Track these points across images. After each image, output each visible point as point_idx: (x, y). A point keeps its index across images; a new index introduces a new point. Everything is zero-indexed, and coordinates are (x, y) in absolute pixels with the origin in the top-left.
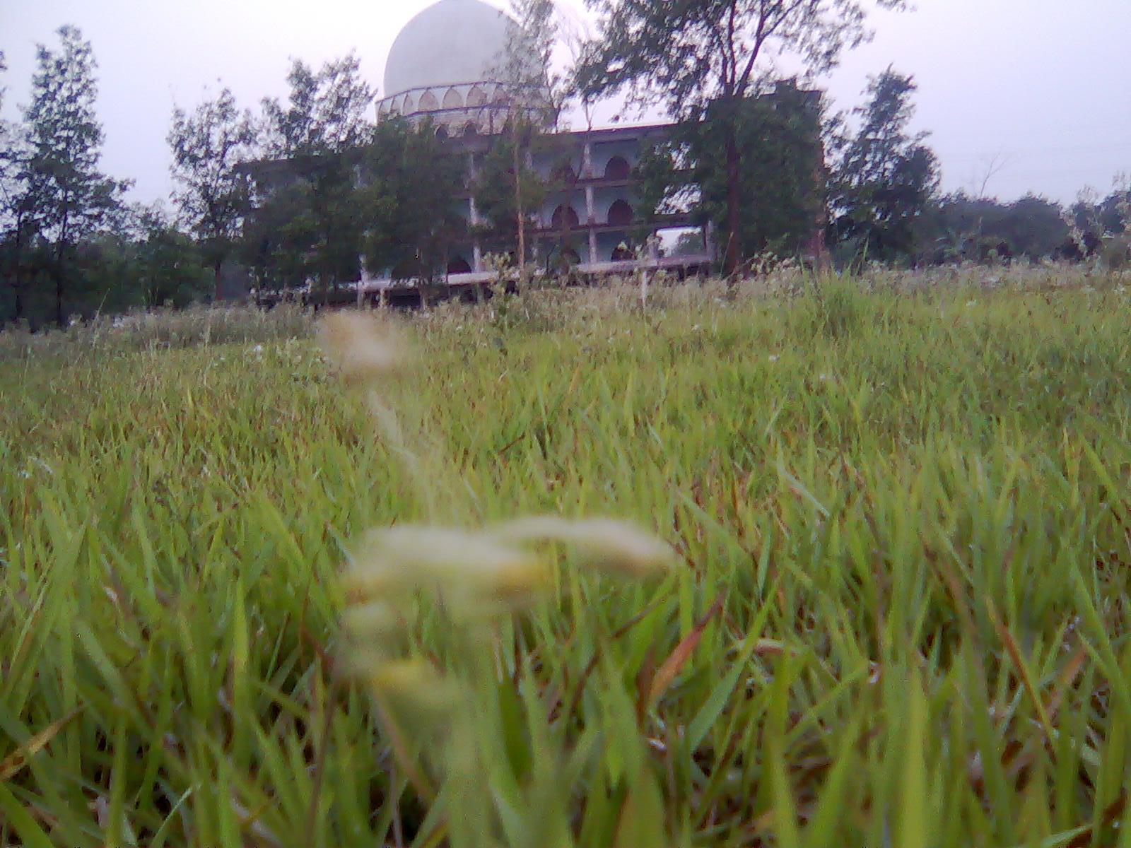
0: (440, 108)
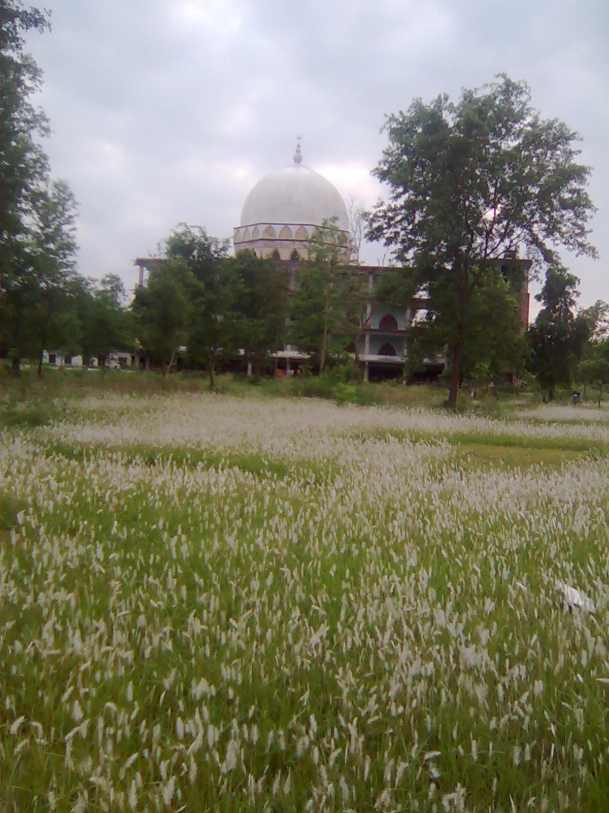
0: (277, 238)
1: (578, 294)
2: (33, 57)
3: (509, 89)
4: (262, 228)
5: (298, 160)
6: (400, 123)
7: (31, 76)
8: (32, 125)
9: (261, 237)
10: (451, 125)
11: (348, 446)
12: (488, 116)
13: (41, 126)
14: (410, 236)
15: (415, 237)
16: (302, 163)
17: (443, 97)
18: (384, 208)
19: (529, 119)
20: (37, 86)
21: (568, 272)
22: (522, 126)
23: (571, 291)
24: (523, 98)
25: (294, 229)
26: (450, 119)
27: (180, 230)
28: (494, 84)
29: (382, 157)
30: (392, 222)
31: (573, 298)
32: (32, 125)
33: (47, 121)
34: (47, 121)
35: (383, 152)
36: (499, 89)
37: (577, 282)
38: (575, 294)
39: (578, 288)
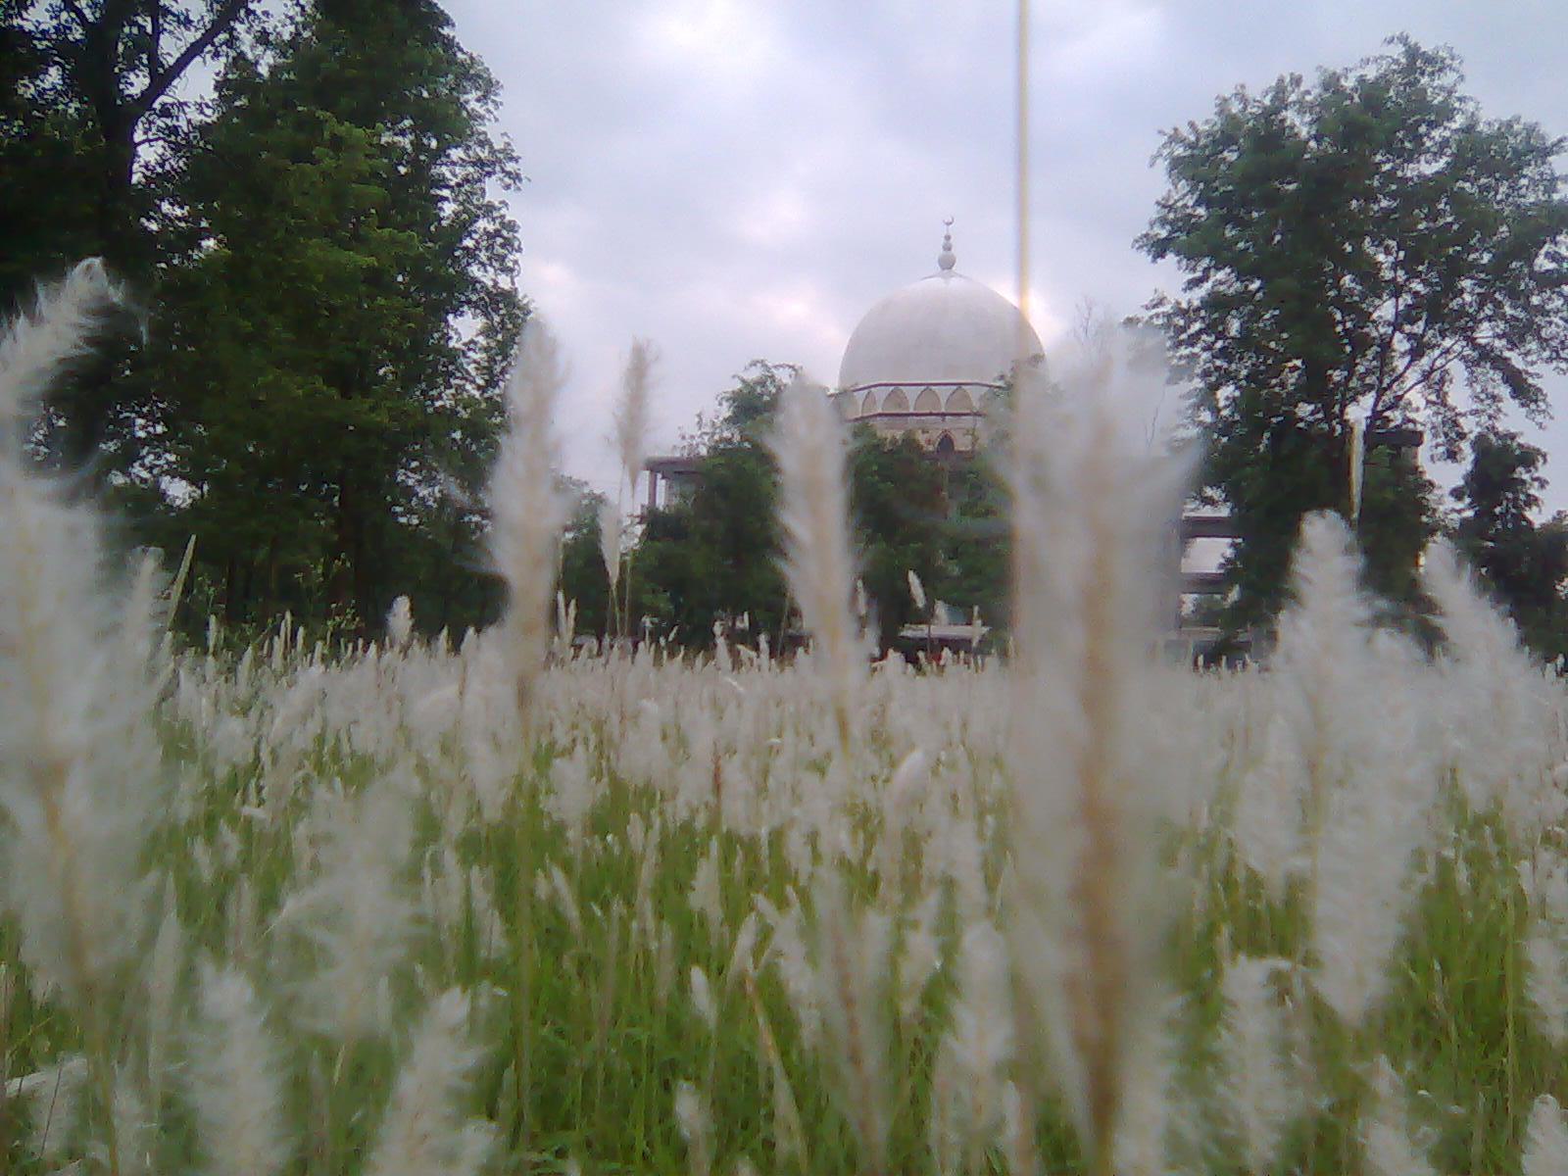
0: (911, 411)
1: (1543, 483)
2: (483, 60)
3: (1417, 62)
4: (881, 394)
5: (947, 264)
6: (1192, 146)
7: (479, 93)
8: (487, 169)
9: (880, 411)
10: (1304, 132)
11: (658, 1146)
12: (1378, 116)
13: (503, 171)
14: (1218, 363)
15: (1230, 363)
16: (954, 268)
17: (1288, 80)
18: (1167, 308)
19: (1459, 121)
20: (489, 111)
21: (1521, 440)
22: (1447, 134)
23: (1526, 477)
24: (1447, 79)
25: (944, 393)
26: (1300, 124)
27: (754, 374)
28: (1382, 57)
29: (1154, 212)
30: (1184, 336)
31: (1532, 492)
32: (487, 169)
33: (516, 160)
34: (516, 160)
35: (1158, 203)
36: (1394, 67)
37: (1540, 458)
38: (1536, 484)
39: (1542, 471)
